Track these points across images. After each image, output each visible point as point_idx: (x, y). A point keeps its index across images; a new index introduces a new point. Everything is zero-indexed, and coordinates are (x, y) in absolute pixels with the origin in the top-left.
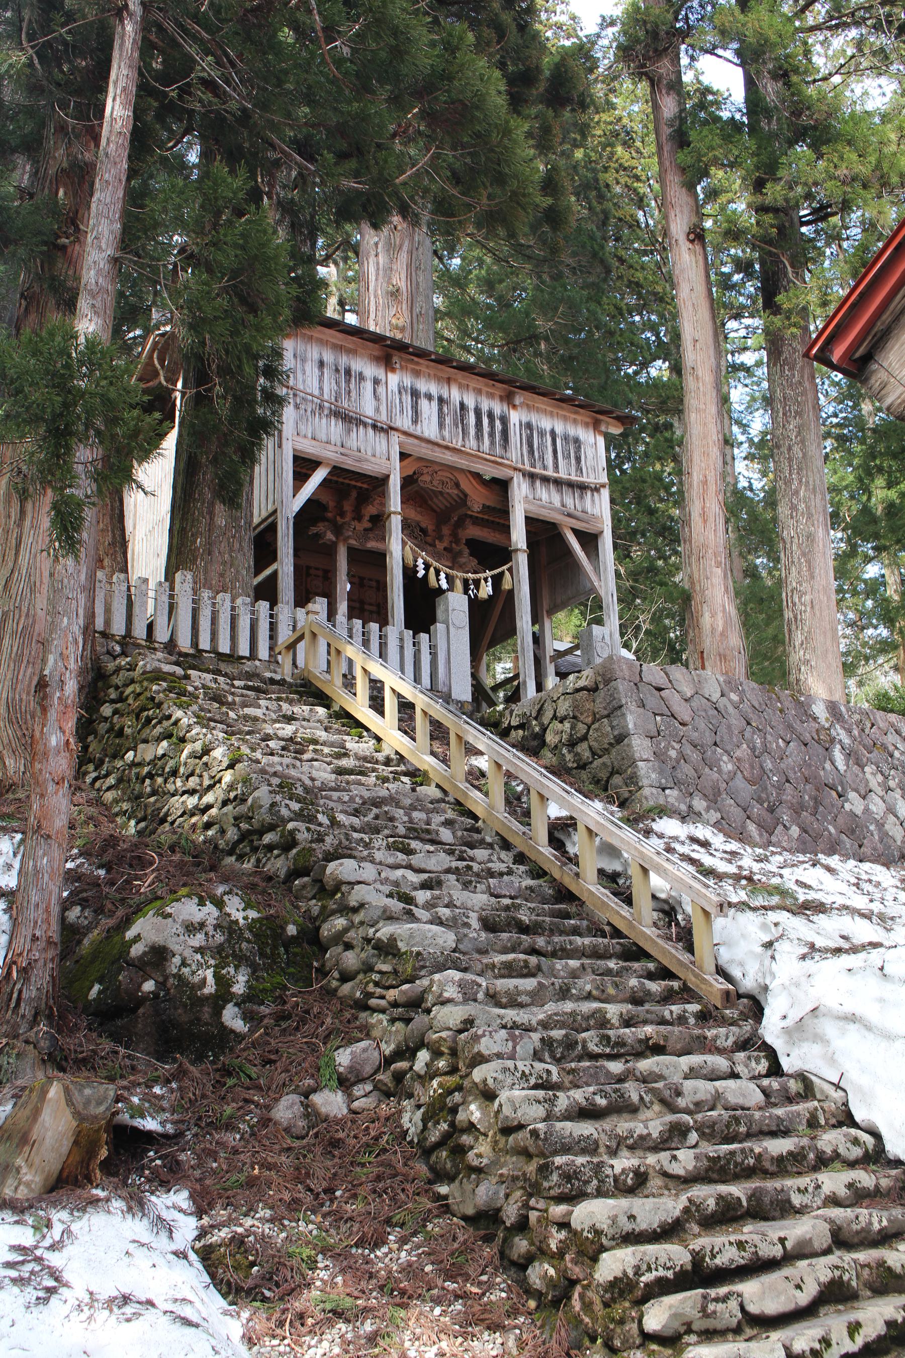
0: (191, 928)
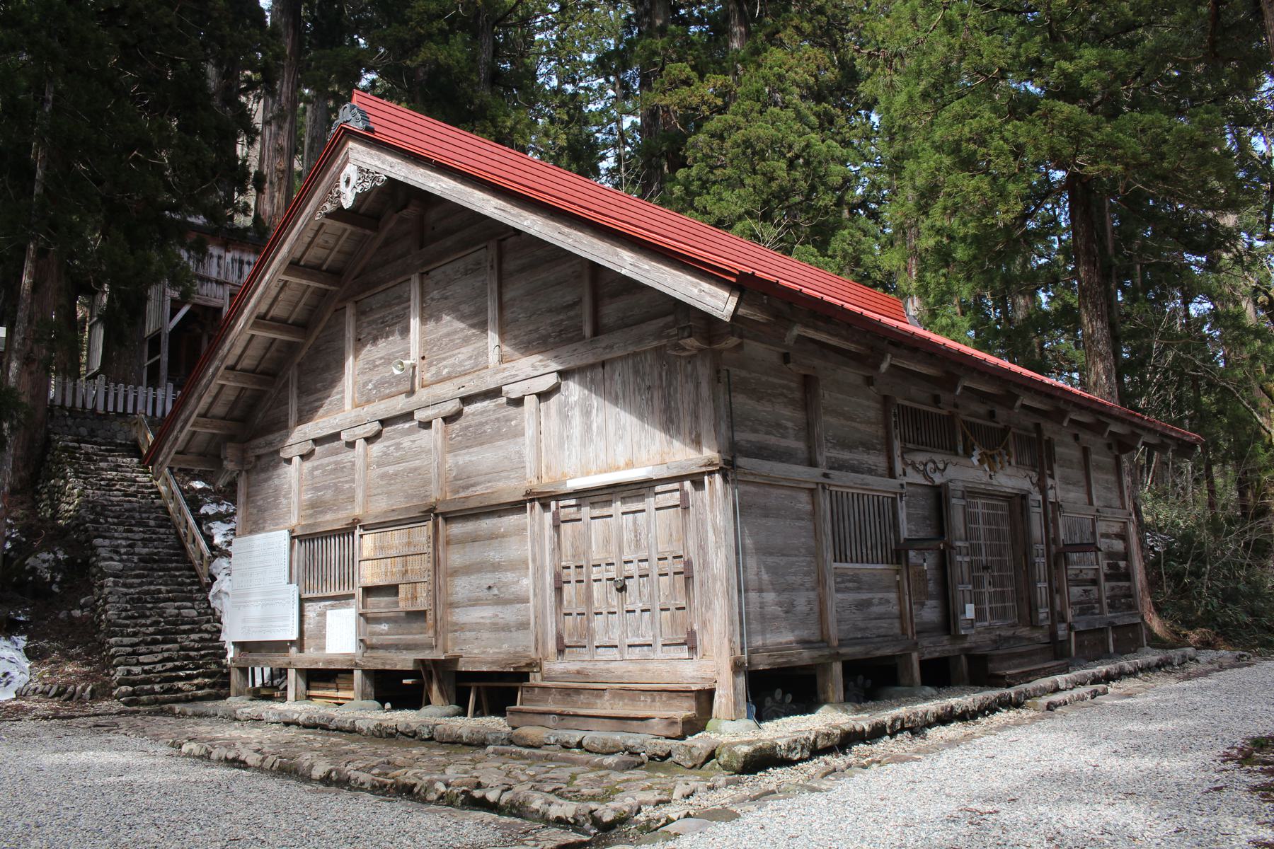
0: (44, 561)
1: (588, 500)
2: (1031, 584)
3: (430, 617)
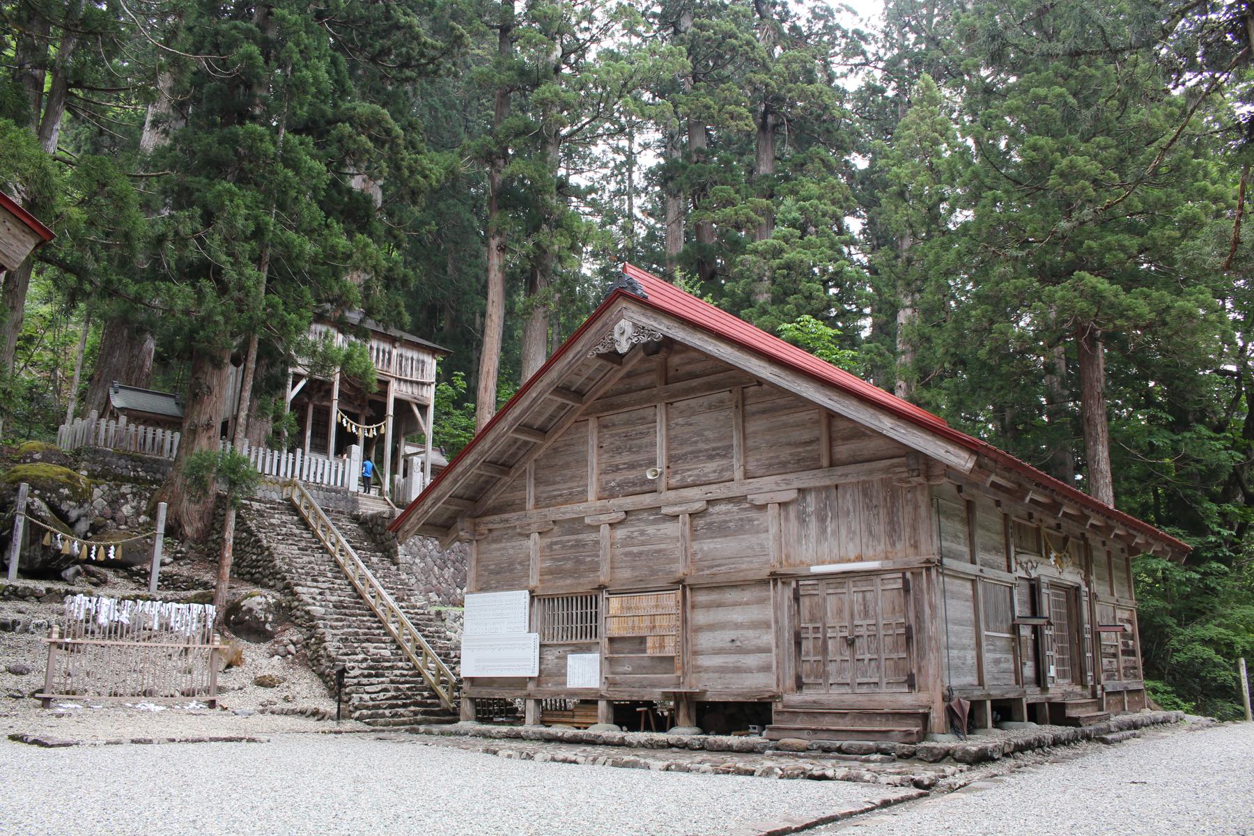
0: (259, 604)
1: (824, 582)
2: (1081, 654)
3: (678, 663)
